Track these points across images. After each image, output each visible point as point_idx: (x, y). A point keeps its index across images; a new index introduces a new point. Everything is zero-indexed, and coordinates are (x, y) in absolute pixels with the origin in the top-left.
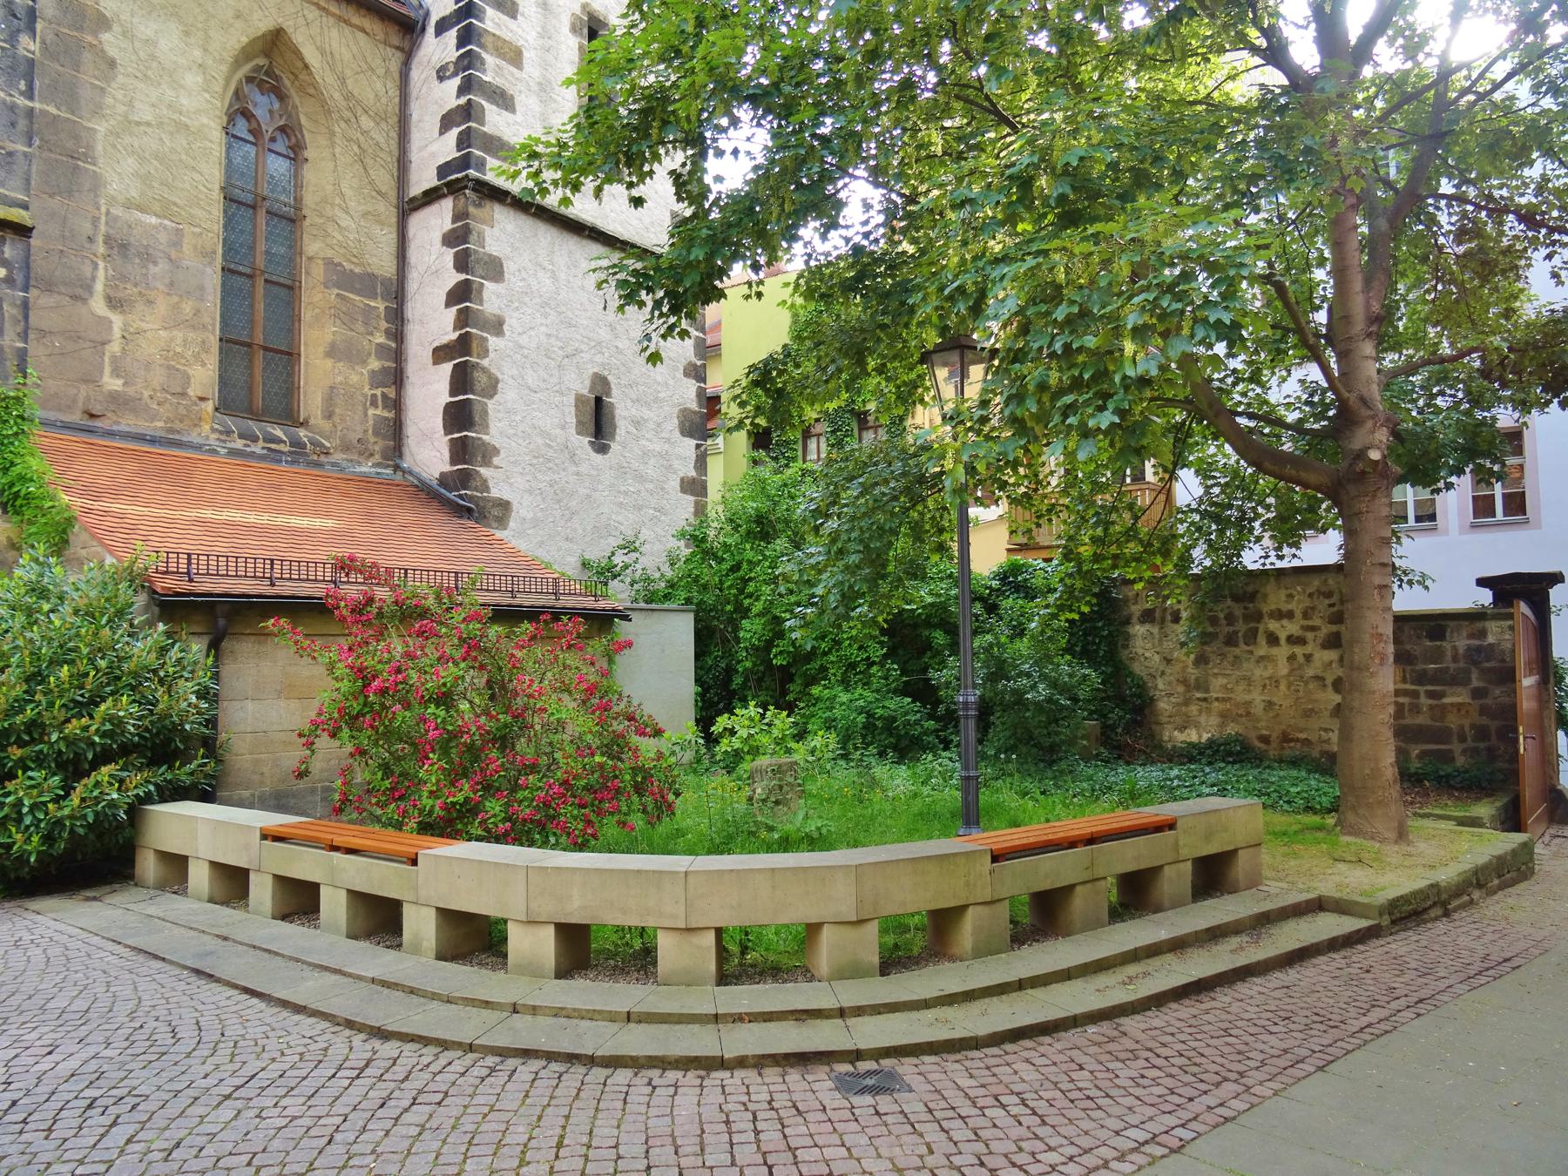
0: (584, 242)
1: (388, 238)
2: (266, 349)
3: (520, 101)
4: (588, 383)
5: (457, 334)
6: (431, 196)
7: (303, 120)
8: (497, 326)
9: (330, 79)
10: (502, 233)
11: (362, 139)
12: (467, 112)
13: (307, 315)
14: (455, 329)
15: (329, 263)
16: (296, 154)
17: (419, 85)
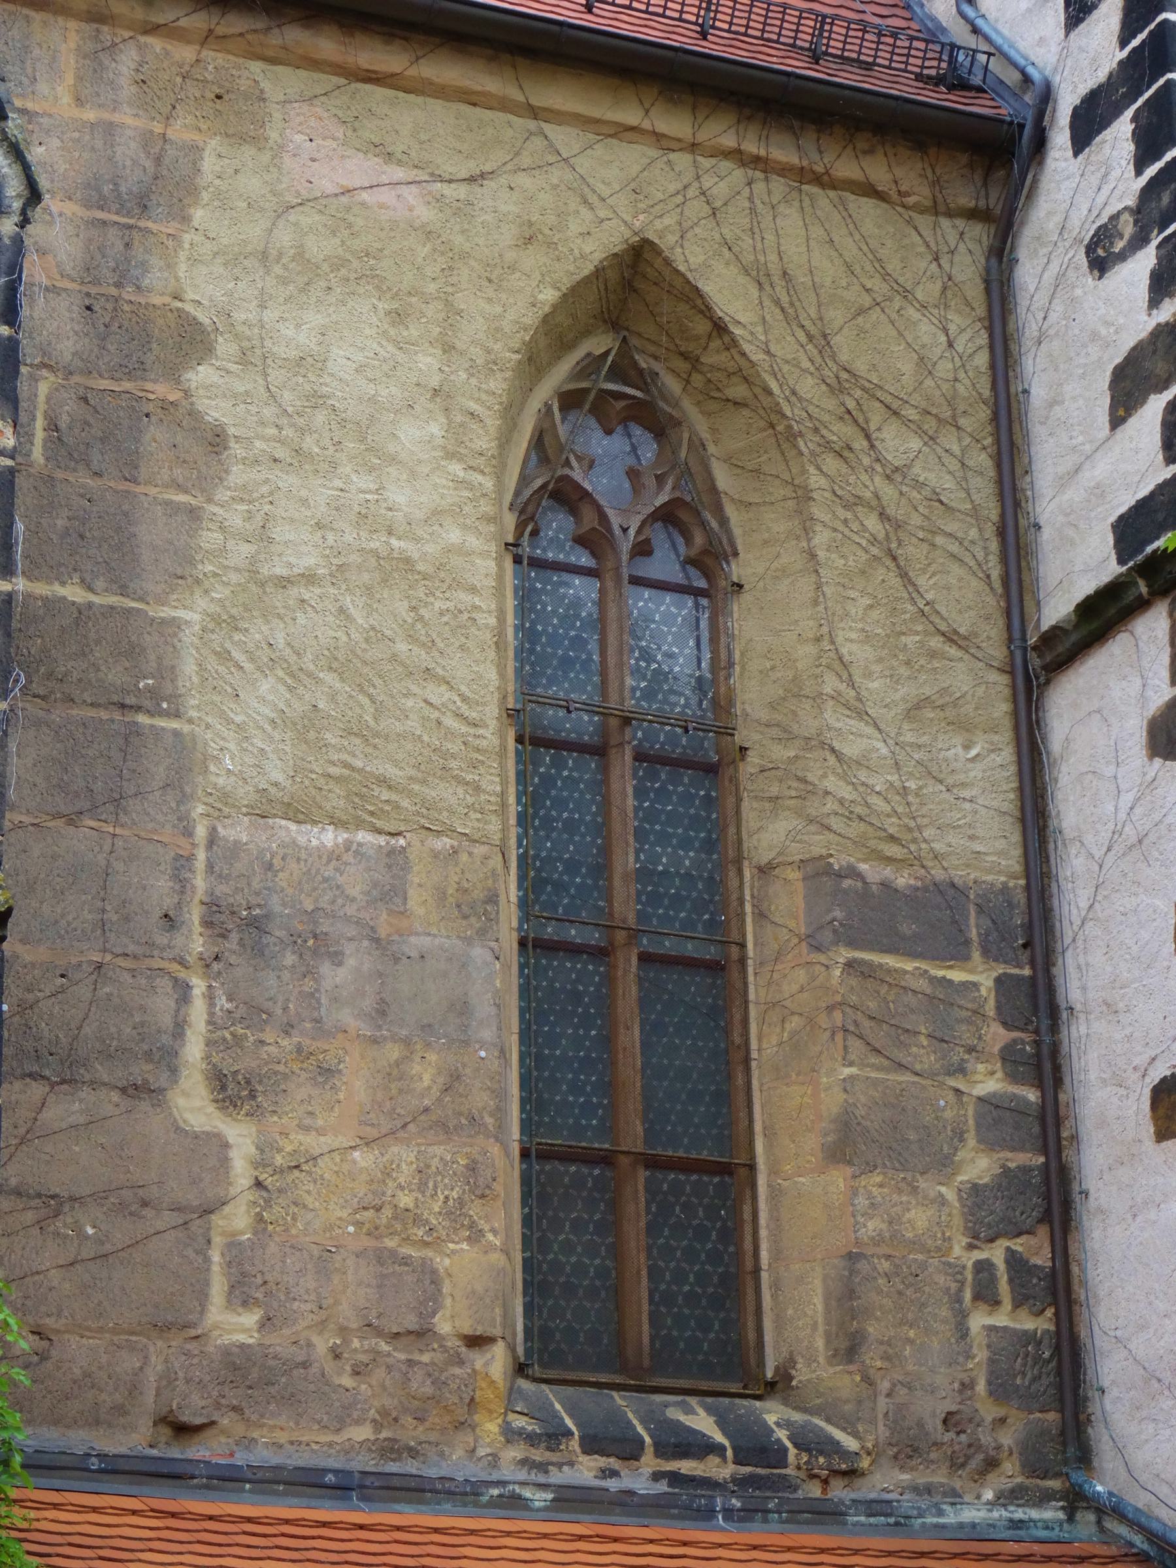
1: (988, 764)
2: (653, 1163)
6: (1104, 615)
7: (723, 478)
9: (787, 346)
11: (888, 492)
13: (765, 1042)
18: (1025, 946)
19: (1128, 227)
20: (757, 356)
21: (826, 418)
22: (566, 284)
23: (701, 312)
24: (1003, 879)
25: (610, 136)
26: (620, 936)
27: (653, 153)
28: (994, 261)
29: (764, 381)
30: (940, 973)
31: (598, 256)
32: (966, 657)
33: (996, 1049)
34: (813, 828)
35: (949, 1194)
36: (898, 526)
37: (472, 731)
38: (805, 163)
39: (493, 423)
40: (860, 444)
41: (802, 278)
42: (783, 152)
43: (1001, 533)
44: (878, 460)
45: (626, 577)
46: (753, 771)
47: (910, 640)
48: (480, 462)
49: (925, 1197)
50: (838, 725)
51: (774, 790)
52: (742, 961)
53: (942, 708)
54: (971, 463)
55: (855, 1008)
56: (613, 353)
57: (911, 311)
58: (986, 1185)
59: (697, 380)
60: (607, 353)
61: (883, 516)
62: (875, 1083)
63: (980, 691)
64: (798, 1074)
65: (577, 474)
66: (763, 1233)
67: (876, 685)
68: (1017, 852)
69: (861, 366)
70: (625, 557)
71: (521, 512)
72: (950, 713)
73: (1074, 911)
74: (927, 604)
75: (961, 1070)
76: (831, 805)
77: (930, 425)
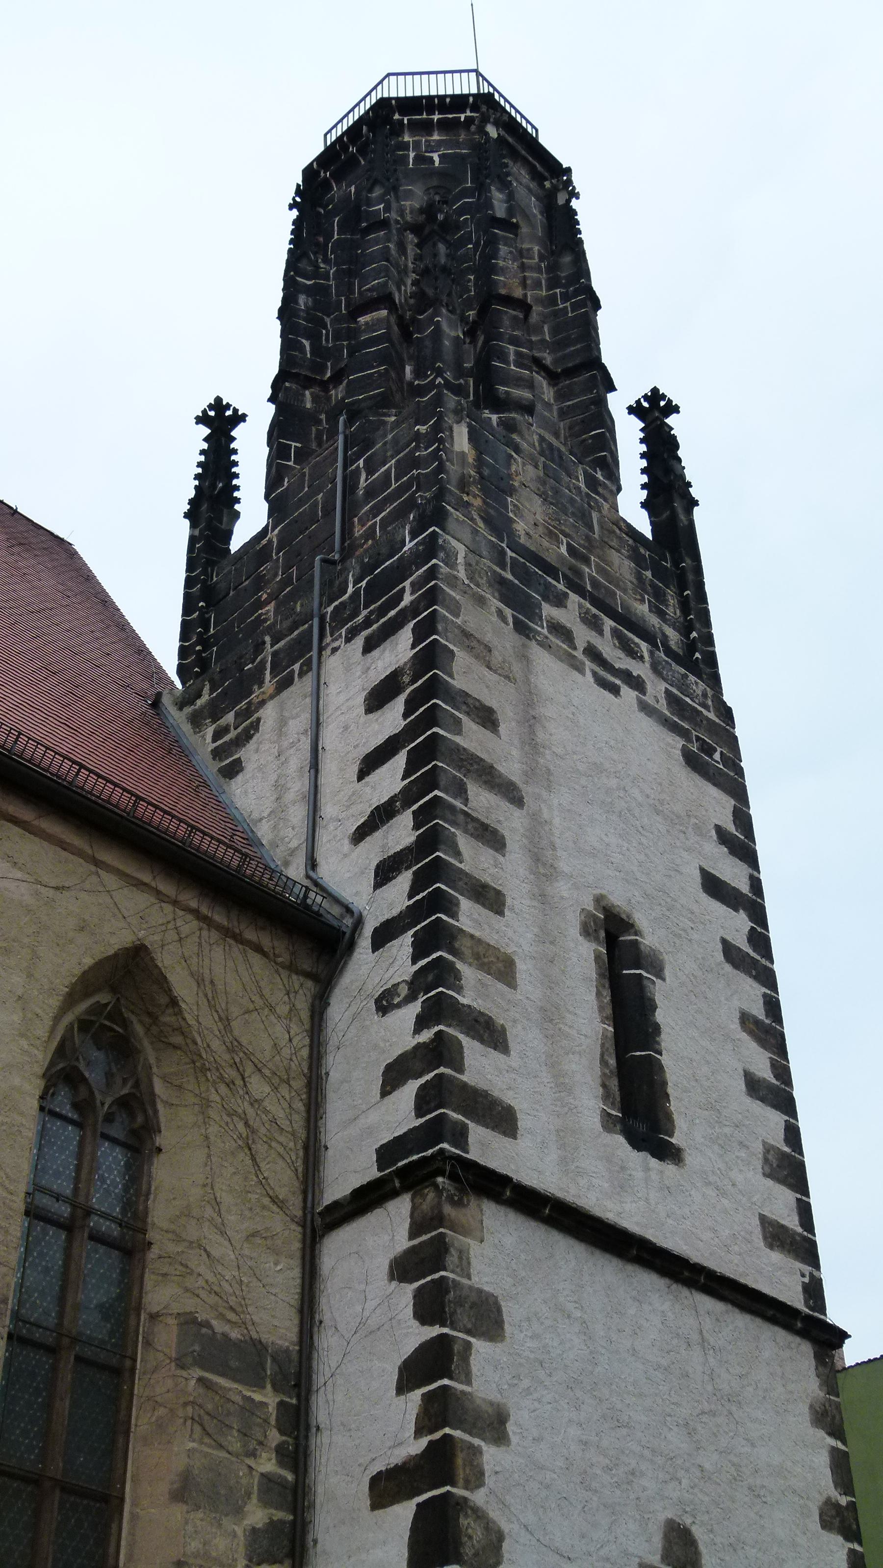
0: (630, 1268)
1: (285, 1275)
2: (66, 1489)
3: (513, 1034)
4: (657, 1541)
5: (424, 1442)
6: (366, 1199)
7: (159, 1087)
8: (495, 1426)
9: (208, 1020)
10: (497, 1251)
11: (250, 1112)
12: (440, 1052)
13: (142, 1421)
14: (419, 1432)
15: (190, 1323)
16: (140, 1144)
17: (342, 1026)
18: (295, 1385)
19: (404, 991)
20: (192, 1022)
21: (224, 1064)
22: (99, 957)
23: (165, 991)
24: (287, 1344)
25: (132, 885)
26: (66, 1341)
27: (153, 900)
28: (317, 1002)
29: (194, 1037)
30: (249, 1394)
31: (117, 947)
32: (281, 1212)
33: (274, 1445)
34: (188, 1294)
35: (239, 1531)
36: (253, 1131)
37: (9, 1197)
38: (230, 926)
39: (49, 1023)
40: (239, 1082)
41: (220, 987)
42: (219, 918)
43: (306, 1148)
44: (247, 1093)
45: (99, 1131)
46: (153, 1257)
47: (253, 1197)
48: (38, 1042)
49: (226, 1531)
50: (211, 1237)
51: (165, 1270)
52: (133, 1370)
53: (265, 1238)
54: (294, 1107)
55: (200, 1406)
56: (111, 1005)
57: (272, 1017)
58: (259, 1529)
59: (155, 1030)
60: (107, 1005)
61: (246, 1124)
62: (206, 1455)
63: (287, 1233)
64: (159, 1444)
65: (82, 1066)
66: (123, 1543)
67: (233, 1218)
68: (296, 1330)
69: (244, 1042)
70: (100, 1119)
71: (49, 1080)
72: (269, 1242)
73: (327, 1369)
74: (264, 1178)
75: (253, 1454)
76: (201, 1282)
77: (276, 1081)
